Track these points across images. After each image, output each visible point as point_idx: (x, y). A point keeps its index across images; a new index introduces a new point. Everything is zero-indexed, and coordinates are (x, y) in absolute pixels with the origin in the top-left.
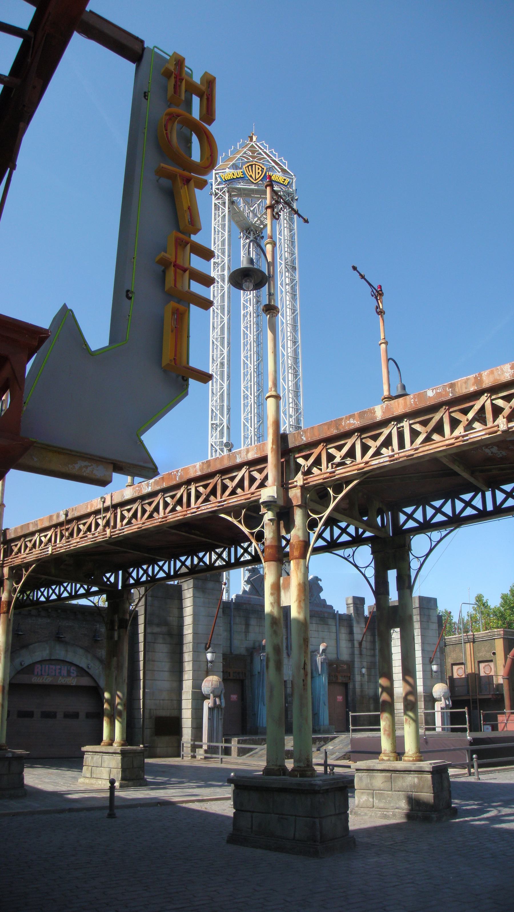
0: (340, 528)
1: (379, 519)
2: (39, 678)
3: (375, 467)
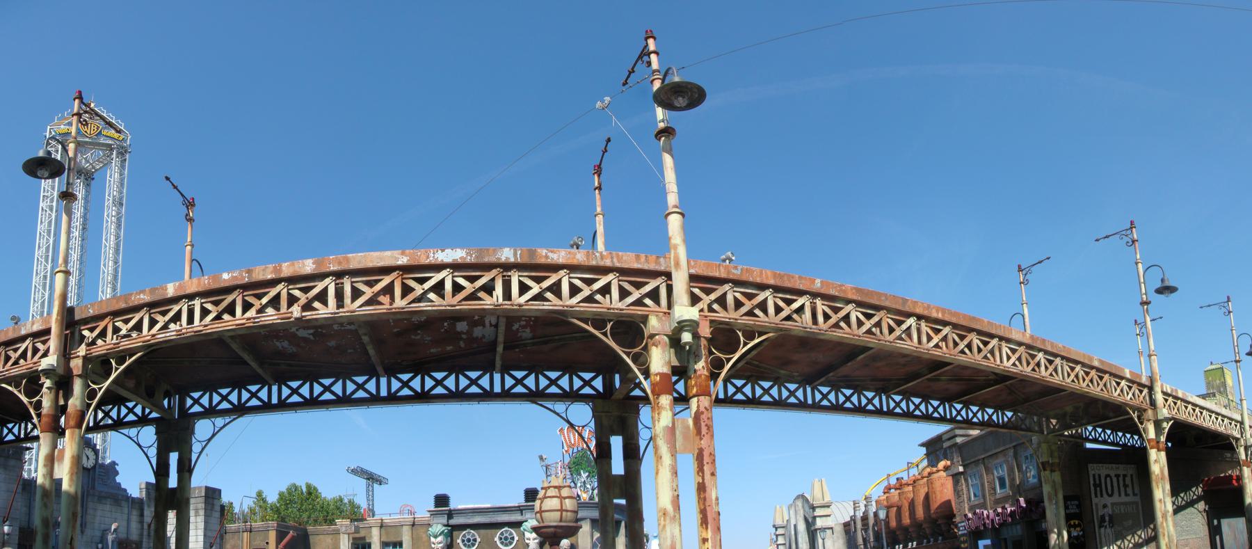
0: (127, 407)
1: (166, 402)
3: (161, 340)
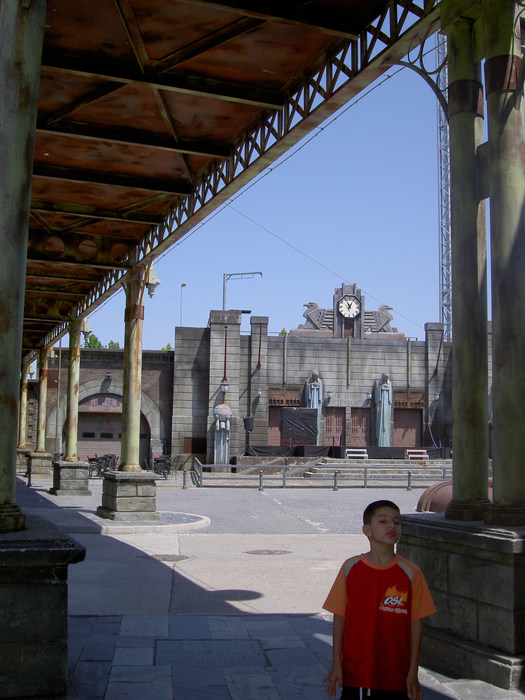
2: (95, 407)
